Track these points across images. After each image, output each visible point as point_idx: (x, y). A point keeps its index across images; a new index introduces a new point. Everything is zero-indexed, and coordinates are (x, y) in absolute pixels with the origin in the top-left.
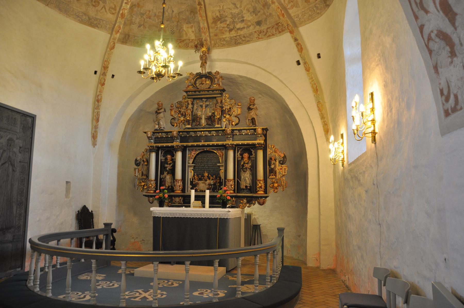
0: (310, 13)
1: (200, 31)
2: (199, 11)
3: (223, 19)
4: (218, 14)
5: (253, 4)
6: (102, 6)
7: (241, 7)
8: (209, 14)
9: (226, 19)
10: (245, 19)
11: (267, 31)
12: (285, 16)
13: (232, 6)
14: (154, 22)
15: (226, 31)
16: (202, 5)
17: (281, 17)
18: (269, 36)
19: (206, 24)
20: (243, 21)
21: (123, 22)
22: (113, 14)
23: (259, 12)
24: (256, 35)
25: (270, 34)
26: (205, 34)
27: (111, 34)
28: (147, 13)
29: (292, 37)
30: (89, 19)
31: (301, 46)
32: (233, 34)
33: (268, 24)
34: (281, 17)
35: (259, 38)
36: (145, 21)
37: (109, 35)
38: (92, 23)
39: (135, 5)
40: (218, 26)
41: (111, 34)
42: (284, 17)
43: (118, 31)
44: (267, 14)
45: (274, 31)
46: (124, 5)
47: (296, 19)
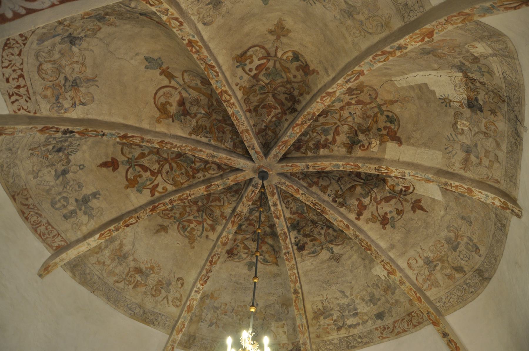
0: (459, 294)
1: (295, 331)
2: (295, 302)
3: (327, 313)
4: (320, 306)
5: (369, 290)
6: (164, 296)
7: (351, 295)
8: (309, 307)
9: (332, 312)
10: (359, 311)
11: (394, 327)
12: (423, 300)
13: (338, 295)
14: (230, 320)
15: (333, 330)
16: (299, 293)
17: (416, 303)
18: (399, 333)
19: (304, 320)
20: (356, 314)
21: (189, 318)
22: (177, 306)
23: (379, 300)
24: (377, 333)
25: (399, 330)
26: (304, 335)
27: (171, 334)
28: (223, 307)
29: (438, 331)
30: (144, 312)
31: (456, 344)
32: (343, 333)
33: (394, 315)
34: (416, 303)
35: (383, 338)
36: (219, 318)
37: (168, 336)
38: (147, 318)
39: (207, 296)
40: (321, 323)
41: (171, 334)
42: (420, 301)
43: (181, 330)
44: (391, 302)
45: (405, 324)
46: (193, 293)
47: (438, 305)
